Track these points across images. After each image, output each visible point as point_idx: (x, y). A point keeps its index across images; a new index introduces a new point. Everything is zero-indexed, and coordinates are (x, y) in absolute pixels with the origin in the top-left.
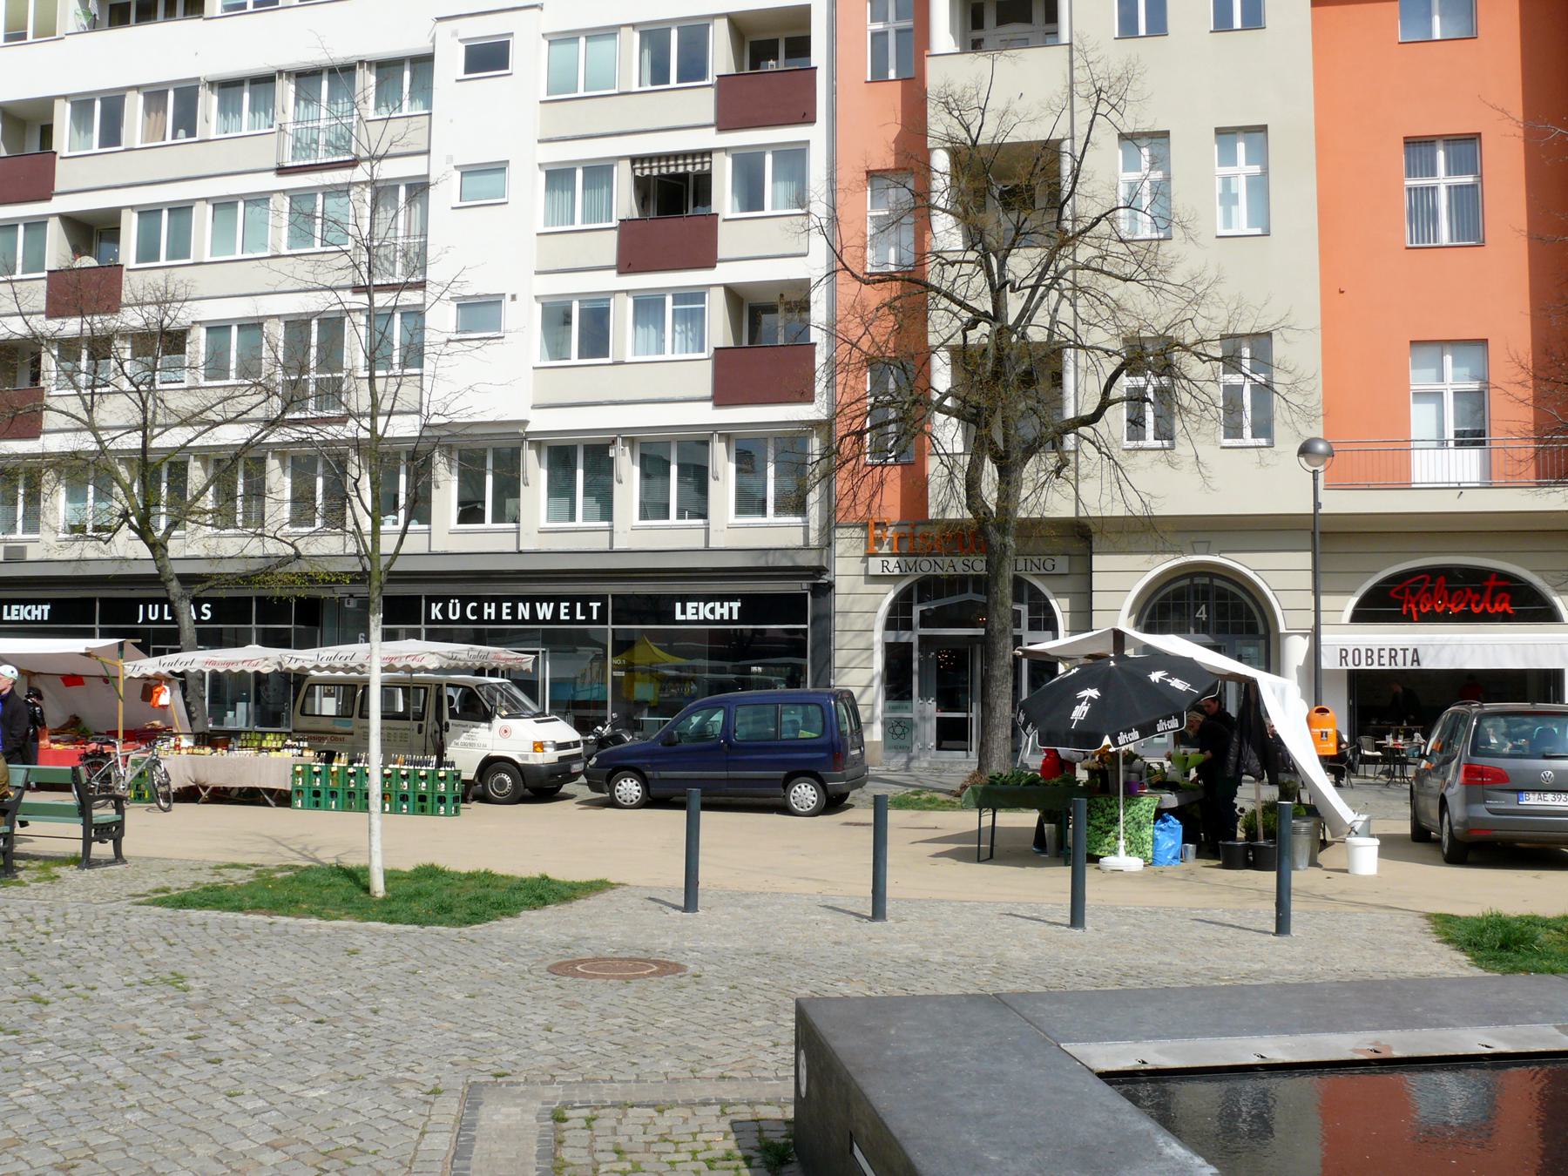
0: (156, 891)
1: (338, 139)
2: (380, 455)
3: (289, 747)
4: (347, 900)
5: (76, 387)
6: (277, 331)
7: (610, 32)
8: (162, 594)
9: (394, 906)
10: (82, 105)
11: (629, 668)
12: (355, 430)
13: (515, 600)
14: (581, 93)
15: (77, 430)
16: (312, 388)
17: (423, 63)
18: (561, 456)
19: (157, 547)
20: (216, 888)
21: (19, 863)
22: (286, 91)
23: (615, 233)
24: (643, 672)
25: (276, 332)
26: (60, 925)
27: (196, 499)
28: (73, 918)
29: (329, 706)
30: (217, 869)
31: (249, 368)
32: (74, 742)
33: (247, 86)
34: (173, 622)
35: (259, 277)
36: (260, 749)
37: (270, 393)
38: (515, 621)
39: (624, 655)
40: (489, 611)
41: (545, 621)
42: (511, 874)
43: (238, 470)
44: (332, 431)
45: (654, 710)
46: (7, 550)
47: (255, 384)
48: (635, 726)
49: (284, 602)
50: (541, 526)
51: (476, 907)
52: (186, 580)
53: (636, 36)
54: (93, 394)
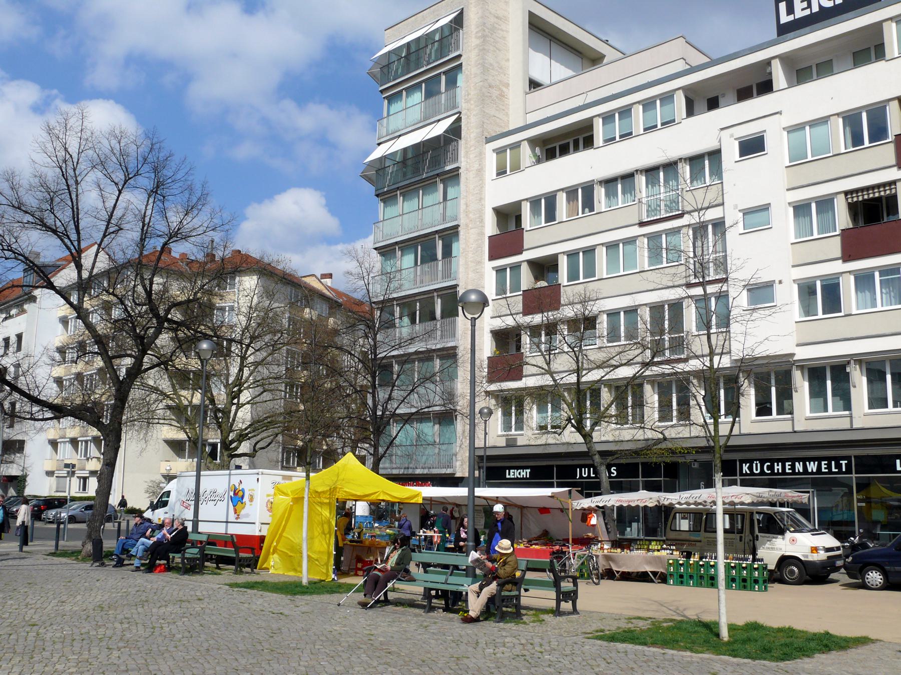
0: (597, 631)
1: (671, 203)
2: (709, 378)
3: (665, 549)
4: (706, 642)
5: (540, 351)
6: (646, 313)
7: (824, 120)
8: (590, 462)
9: (736, 646)
10: (535, 202)
11: (868, 500)
12: (694, 365)
13: (793, 461)
14: (810, 158)
15: (542, 374)
16: (667, 345)
17: (715, 155)
18: (816, 373)
19: (587, 436)
20: (630, 631)
21: (523, 612)
22: (641, 181)
23: (839, 238)
24: (876, 503)
25: (645, 314)
26: (548, 648)
27: (607, 409)
28: (554, 644)
29: (685, 525)
30: (629, 619)
31: (631, 334)
32: (546, 544)
33: (619, 181)
34: (596, 477)
35: (635, 283)
36: (648, 550)
37: (645, 348)
38: (794, 473)
39: (862, 493)
40: (778, 467)
41: (812, 473)
42: (805, 629)
43: (628, 392)
44: (680, 367)
45: (884, 527)
46: (507, 439)
47: (636, 343)
48: (875, 538)
49: (657, 465)
50: (806, 415)
51: (787, 650)
52: (604, 454)
53: (841, 120)
54: (550, 354)
